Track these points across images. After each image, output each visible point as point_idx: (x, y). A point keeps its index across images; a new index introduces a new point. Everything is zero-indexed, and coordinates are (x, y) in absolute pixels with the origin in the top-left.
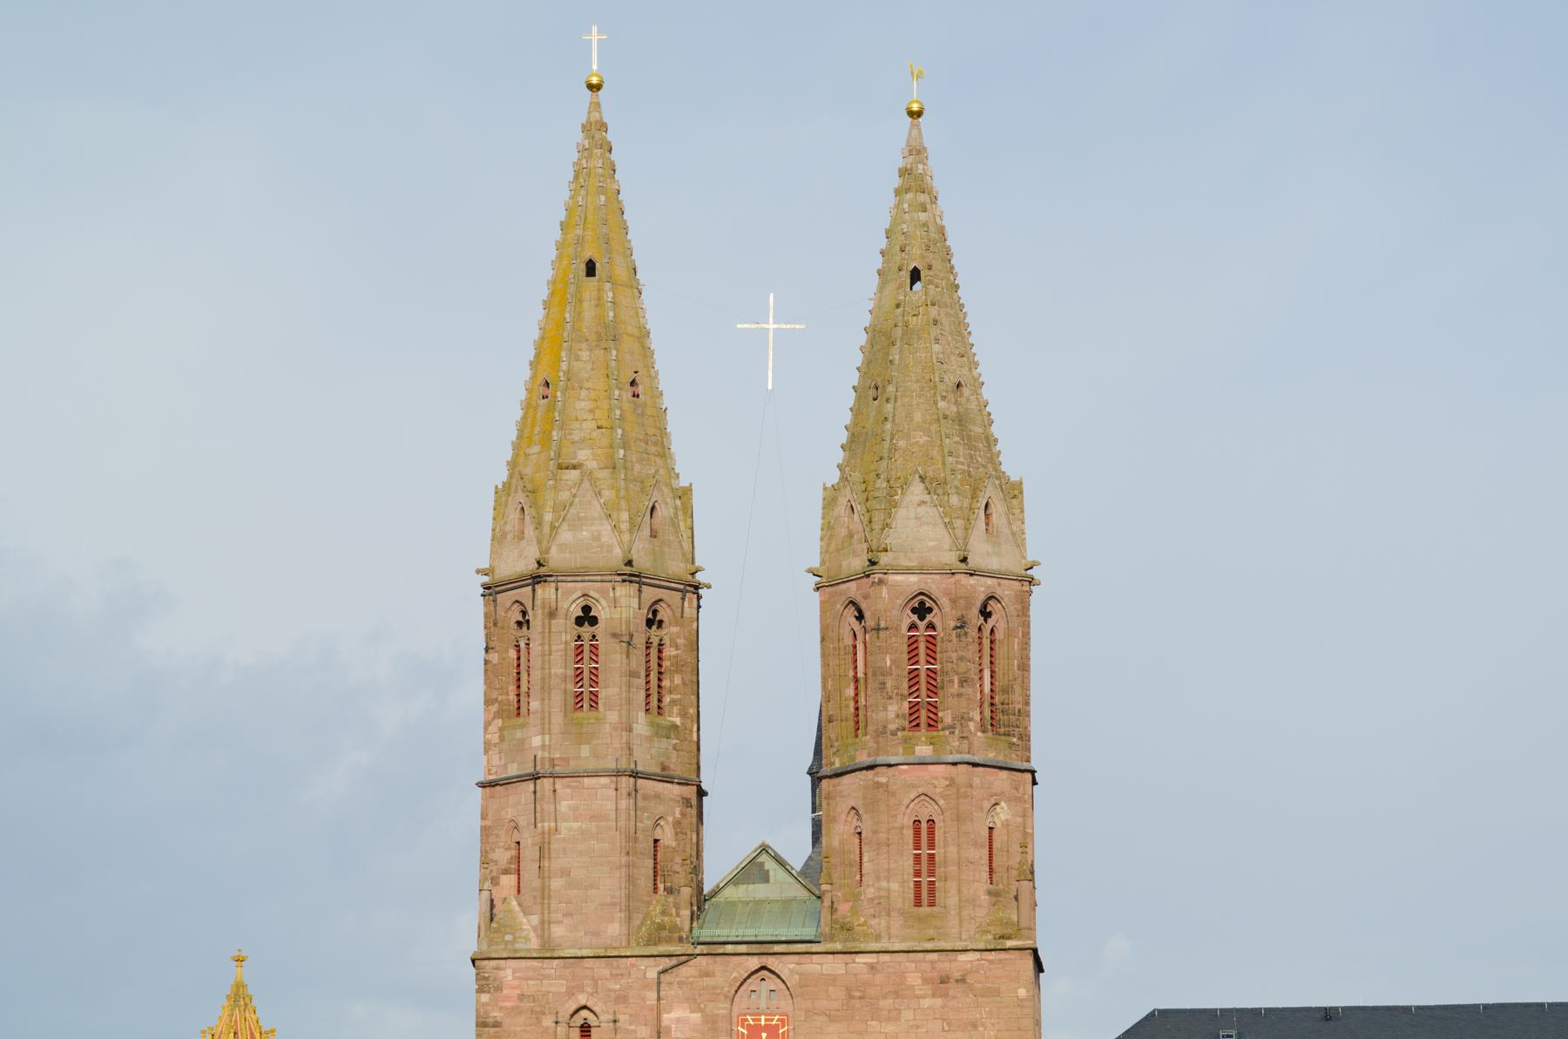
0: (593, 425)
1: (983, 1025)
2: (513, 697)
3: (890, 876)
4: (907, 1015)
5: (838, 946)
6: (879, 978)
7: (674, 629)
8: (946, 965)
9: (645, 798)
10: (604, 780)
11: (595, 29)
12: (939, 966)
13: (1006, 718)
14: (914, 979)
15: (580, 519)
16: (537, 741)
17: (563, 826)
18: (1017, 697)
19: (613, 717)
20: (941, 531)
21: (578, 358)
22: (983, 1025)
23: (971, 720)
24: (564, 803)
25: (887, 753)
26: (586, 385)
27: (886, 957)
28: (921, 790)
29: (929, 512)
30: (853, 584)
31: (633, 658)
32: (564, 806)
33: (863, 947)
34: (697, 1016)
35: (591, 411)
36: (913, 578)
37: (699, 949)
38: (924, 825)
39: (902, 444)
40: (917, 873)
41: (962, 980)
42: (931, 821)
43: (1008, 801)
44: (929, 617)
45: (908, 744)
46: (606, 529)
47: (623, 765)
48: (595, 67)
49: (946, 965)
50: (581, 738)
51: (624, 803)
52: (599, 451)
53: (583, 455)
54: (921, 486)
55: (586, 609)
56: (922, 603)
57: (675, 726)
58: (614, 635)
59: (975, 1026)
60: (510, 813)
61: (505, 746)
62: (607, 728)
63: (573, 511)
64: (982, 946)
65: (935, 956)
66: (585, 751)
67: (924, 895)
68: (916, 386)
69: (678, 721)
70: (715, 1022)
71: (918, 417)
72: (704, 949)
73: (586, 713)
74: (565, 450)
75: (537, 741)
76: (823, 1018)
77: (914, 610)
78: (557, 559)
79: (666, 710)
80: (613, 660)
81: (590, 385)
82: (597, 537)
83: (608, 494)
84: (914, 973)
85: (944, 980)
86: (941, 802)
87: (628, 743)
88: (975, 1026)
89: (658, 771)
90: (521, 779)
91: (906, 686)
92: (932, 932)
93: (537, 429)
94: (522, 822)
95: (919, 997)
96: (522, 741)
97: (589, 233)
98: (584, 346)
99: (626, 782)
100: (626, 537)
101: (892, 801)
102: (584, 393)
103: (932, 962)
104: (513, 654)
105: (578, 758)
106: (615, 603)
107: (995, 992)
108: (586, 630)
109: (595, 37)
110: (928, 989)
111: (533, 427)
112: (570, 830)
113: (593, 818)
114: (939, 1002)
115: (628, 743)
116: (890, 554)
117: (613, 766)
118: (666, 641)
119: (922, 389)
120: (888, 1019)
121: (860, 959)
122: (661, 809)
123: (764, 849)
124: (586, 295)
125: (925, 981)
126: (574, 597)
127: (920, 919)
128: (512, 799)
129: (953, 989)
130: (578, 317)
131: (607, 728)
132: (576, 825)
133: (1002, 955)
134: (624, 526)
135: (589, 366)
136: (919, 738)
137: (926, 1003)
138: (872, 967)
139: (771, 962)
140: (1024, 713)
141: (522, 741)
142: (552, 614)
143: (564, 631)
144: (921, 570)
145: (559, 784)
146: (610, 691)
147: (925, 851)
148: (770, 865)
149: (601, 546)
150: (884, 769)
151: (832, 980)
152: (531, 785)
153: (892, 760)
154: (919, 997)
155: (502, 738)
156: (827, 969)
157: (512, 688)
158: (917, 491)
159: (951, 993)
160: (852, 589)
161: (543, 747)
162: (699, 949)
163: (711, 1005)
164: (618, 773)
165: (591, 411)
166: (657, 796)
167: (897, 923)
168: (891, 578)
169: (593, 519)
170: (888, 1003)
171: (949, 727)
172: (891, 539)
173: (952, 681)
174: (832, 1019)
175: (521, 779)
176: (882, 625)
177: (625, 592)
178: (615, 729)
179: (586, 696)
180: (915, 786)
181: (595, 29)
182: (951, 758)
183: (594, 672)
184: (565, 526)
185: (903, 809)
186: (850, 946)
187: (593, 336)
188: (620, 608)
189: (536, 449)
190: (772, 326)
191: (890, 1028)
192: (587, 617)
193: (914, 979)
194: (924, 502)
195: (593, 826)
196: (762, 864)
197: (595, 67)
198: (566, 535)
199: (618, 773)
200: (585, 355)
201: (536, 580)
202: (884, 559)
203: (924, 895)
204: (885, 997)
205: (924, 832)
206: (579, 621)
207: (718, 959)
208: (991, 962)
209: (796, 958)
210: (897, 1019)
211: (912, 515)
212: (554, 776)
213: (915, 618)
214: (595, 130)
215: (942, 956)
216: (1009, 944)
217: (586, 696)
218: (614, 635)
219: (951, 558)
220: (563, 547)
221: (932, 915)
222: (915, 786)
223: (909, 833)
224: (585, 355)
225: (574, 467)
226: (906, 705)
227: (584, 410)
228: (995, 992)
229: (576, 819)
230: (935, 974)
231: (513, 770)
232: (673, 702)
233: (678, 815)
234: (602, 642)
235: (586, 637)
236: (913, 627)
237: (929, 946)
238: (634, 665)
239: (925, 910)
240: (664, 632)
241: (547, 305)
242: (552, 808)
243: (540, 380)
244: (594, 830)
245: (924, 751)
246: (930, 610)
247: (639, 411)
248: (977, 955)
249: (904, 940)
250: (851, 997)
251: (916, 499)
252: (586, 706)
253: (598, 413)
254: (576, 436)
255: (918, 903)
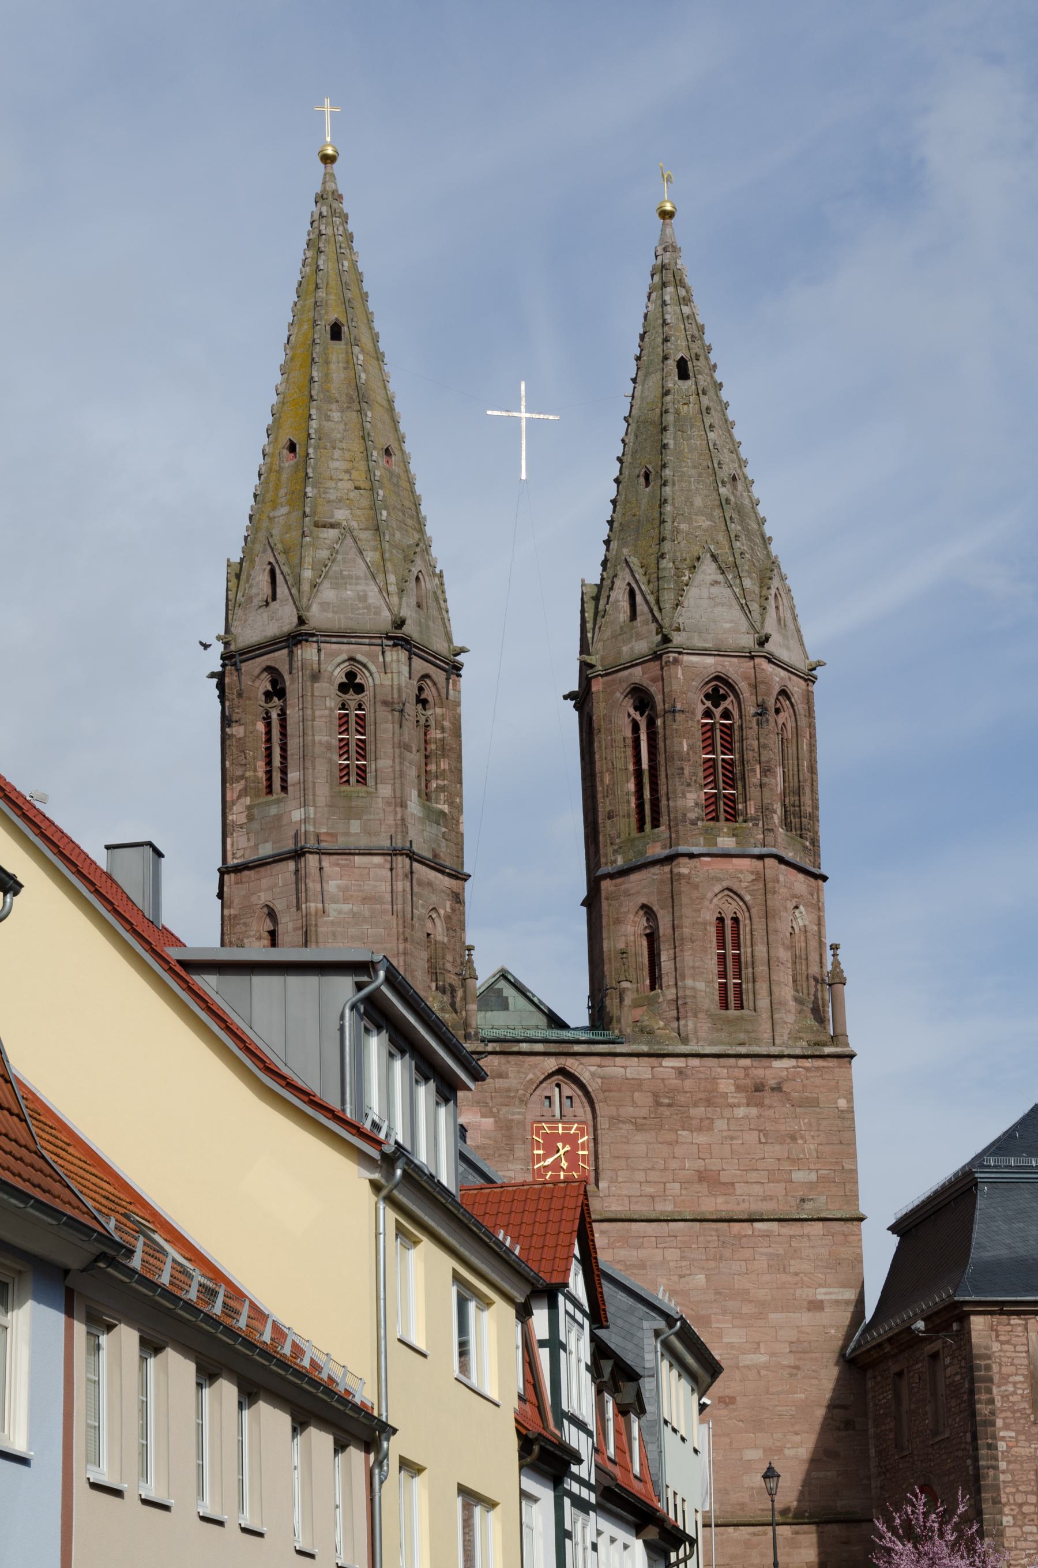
0: (350, 485)
1: (802, 1137)
2: (261, 774)
3: (698, 973)
4: (720, 1124)
5: (645, 1048)
6: (688, 1084)
7: (439, 711)
8: (760, 1072)
9: (420, 883)
10: (377, 860)
11: (327, 101)
12: (754, 1072)
13: (800, 820)
14: (726, 1086)
15: (343, 577)
16: (297, 815)
17: (331, 907)
18: (807, 800)
19: (385, 791)
20: (737, 613)
21: (328, 418)
22: (802, 1137)
23: (775, 812)
24: (332, 883)
25: (686, 843)
26: (339, 445)
27: (695, 1062)
28: (725, 884)
29: (722, 592)
30: (639, 669)
31: (406, 729)
32: (332, 886)
33: (671, 1049)
34: (490, 1121)
35: (347, 471)
36: (710, 660)
37: (490, 1047)
38: (728, 923)
39: (684, 527)
40: (723, 974)
41: (778, 1089)
42: (736, 920)
43: (806, 906)
44: (724, 704)
45: (710, 836)
46: (372, 591)
47: (399, 844)
48: (328, 139)
49: (760, 1072)
50: (351, 813)
51: (399, 886)
52: (359, 512)
53: (341, 515)
54: (714, 566)
55: (351, 675)
56: (716, 689)
57: (442, 813)
58: (385, 703)
59: (793, 1138)
60: (263, 898)
61: (255, 825)
62: (380, 803)
63: (335, 568)
64: (798, 1051)
65: (747, 1062)
66: (355, 826)
67: (733, 997)
68: (693, 472)
69: (445, 808)
70: (509, 1128)
71: (698, 502)
72: (497, 1047)
73: (354, 788)
74: (320, 509)
75: (297, 815)
76: (627, 1126)
77: (707, 696)
78: (318, 617)
79: (433, 796)
80: (385, 730)
81: (344, 445)
82: (363, 598)
83: (371, 556)
84: (726, 1078)
85: (759, 1088)
86: (747, 898)
87: (403, 819)
88: (793, 1138)
89: (429, 856)
90: (278, 859)
91: (701, 774)
92: (742, 1036)
93: (283, 492)
94: (279, 906)
95: (732, 1106)
96: (279, 817)
97: (332, 297)
98: (334, 406)
99: (402, 862)
100: (395, 600)
101: (695, 894)
102: (337, 454)
103: (746, 1068)
104: (261, 727)
105: (347, 834)
106: (385, 668)
107: (814, 1103)
108: (352, 698)
109: (328, 110)
110: (741, 1097)
111: (277, 488)
112: (340, 912)
113: (365, 900)
114: (754, 1111)
115: (403, 819)
116: (683, 634)
117: (386, 843)
118: (432, 723)
119: (700, 475)
120: (700, 1129)
121: (668, 1062)
122: (434, 899)
123: (504, 975)
124: (333, 358)
125: (739, 1088)
126: (339, 659)
127: (728, 1021)
128: (265, 883)
129: (769, 1098)
130: (327, 377)
131: (380, 803)
132: (346, 907)
133: (820, 1063)
134: (393, 589)
135: (341, 427)
136: (720, 829)
137: (740, 1112)
138: (680, 1072)
139: (571, 1064)
140: (814, 817)
141: (279, 817)
142: (315, 677)
143: (326, 702)
144: (718, 652)
145: (326, 861)
146: (383, 763)
147: (731, 952)
148: (509, 992)
149: (368, 608)
150: (686, 860)
151: (638, 1084)
152: (291, 865)
153: (696, 850)
154: (732, 1106)
155: (250, 818)
156: (630, 1073)
157: (261, 765)
158: (708, 570)
159: (767, 1102)
160: (637, 674)
161: (306, 820)
162: (490, 1047)
163: (504, 1109)
164: (394, 853)
165: (347, 471)
166: (430, 884)
167: (704, 1026)
168: (686, 658)
169: (358, 578)
170: (699, 1111)
171: (753, 819)
172: (682, 617)
173: (754, 771)
174: (639, 1128)
175: (278, 859)
176: (679, 707)
177: (397, 657)
178: (389, 804)
179: (353, 771)
180: (719, 880)
181: (327, 101)
182: (757, 851)
183: (362, 745)
184: (326, 584)
185: (706, 903)
186: (656, 1048)
187: (343, 398)
188: (391, 674)
189: (284, 510)
190: (524, 415)
191: (702, 1139)
192: (351, 684)
193: (726, 1086)
194: (717, 582)
195: (366, 910)
196: (500, 991)
197: (328, 139)
198: (328, 593)
199: (394, 853)
200: (336, 416)
201: (294, 639)
202: (677, 639)
203: (733, 997)
204: (695, 1105)
205: (728, 932)
206: (343, 688)
207: (511, 1058)
208: (807, 1069)
209: (597, 1060)
210: (710, 1129)
211: (705, 595)
212: (320, 853)
213: (709, 704)
214: (328, 199)
215: (756, 1062)
216: (827, 1050)
217: (353, 771)
218: (385, 703)
219: (748, 641)
220: (325, 606)
221: (741, 1018)
222: (719, 880)
223: (713, 930)
224: (336, 416)
225: (332, 526)
226: (703, 797)
227: (338, 472)
228: (814, 1103)
229: (346, 901)
230: (748, 1081)
231: (266, 850)
232: (441, 789)
233: (448, 910)
234: (368, 712)
235: (353, 704)
236: (708, 714)
237: (743, 1050)
238: (406, 738)
239: (732, 1013)
240: (429, 712)
241: (284, 370)
242: (318, 887)
243: (284, 441)
244: (367, 914)
245: (726, 842)
246: (724, 697)
247: (395, 480)
248: (793, 1062)
249: (712, 1043)
250: (658, 1104)
251: (709, 579)
252: (353, 779)
253: (355, 474)
254: (332, 495)
255: (725, 1005)
